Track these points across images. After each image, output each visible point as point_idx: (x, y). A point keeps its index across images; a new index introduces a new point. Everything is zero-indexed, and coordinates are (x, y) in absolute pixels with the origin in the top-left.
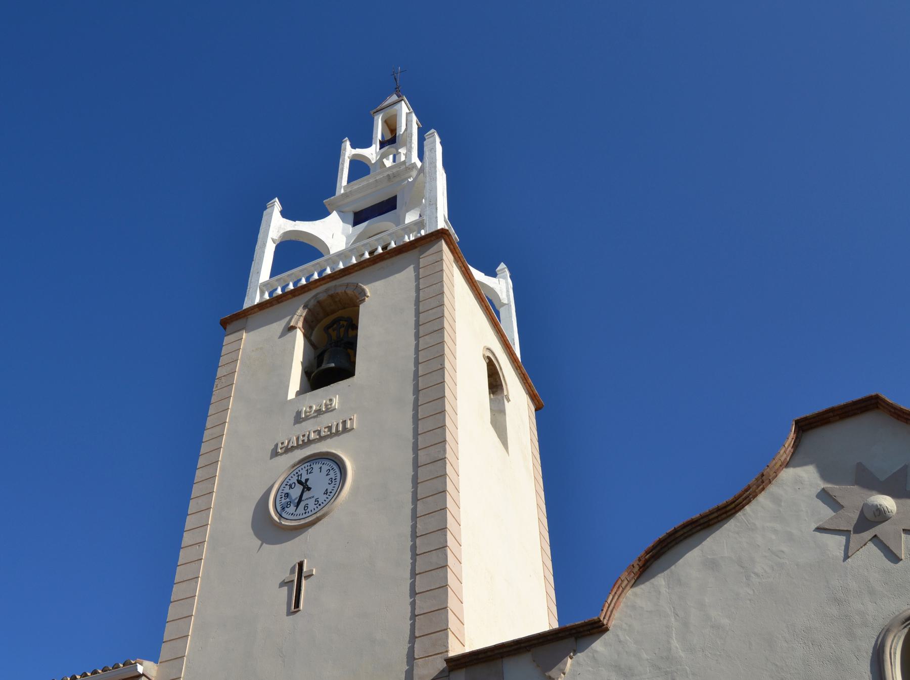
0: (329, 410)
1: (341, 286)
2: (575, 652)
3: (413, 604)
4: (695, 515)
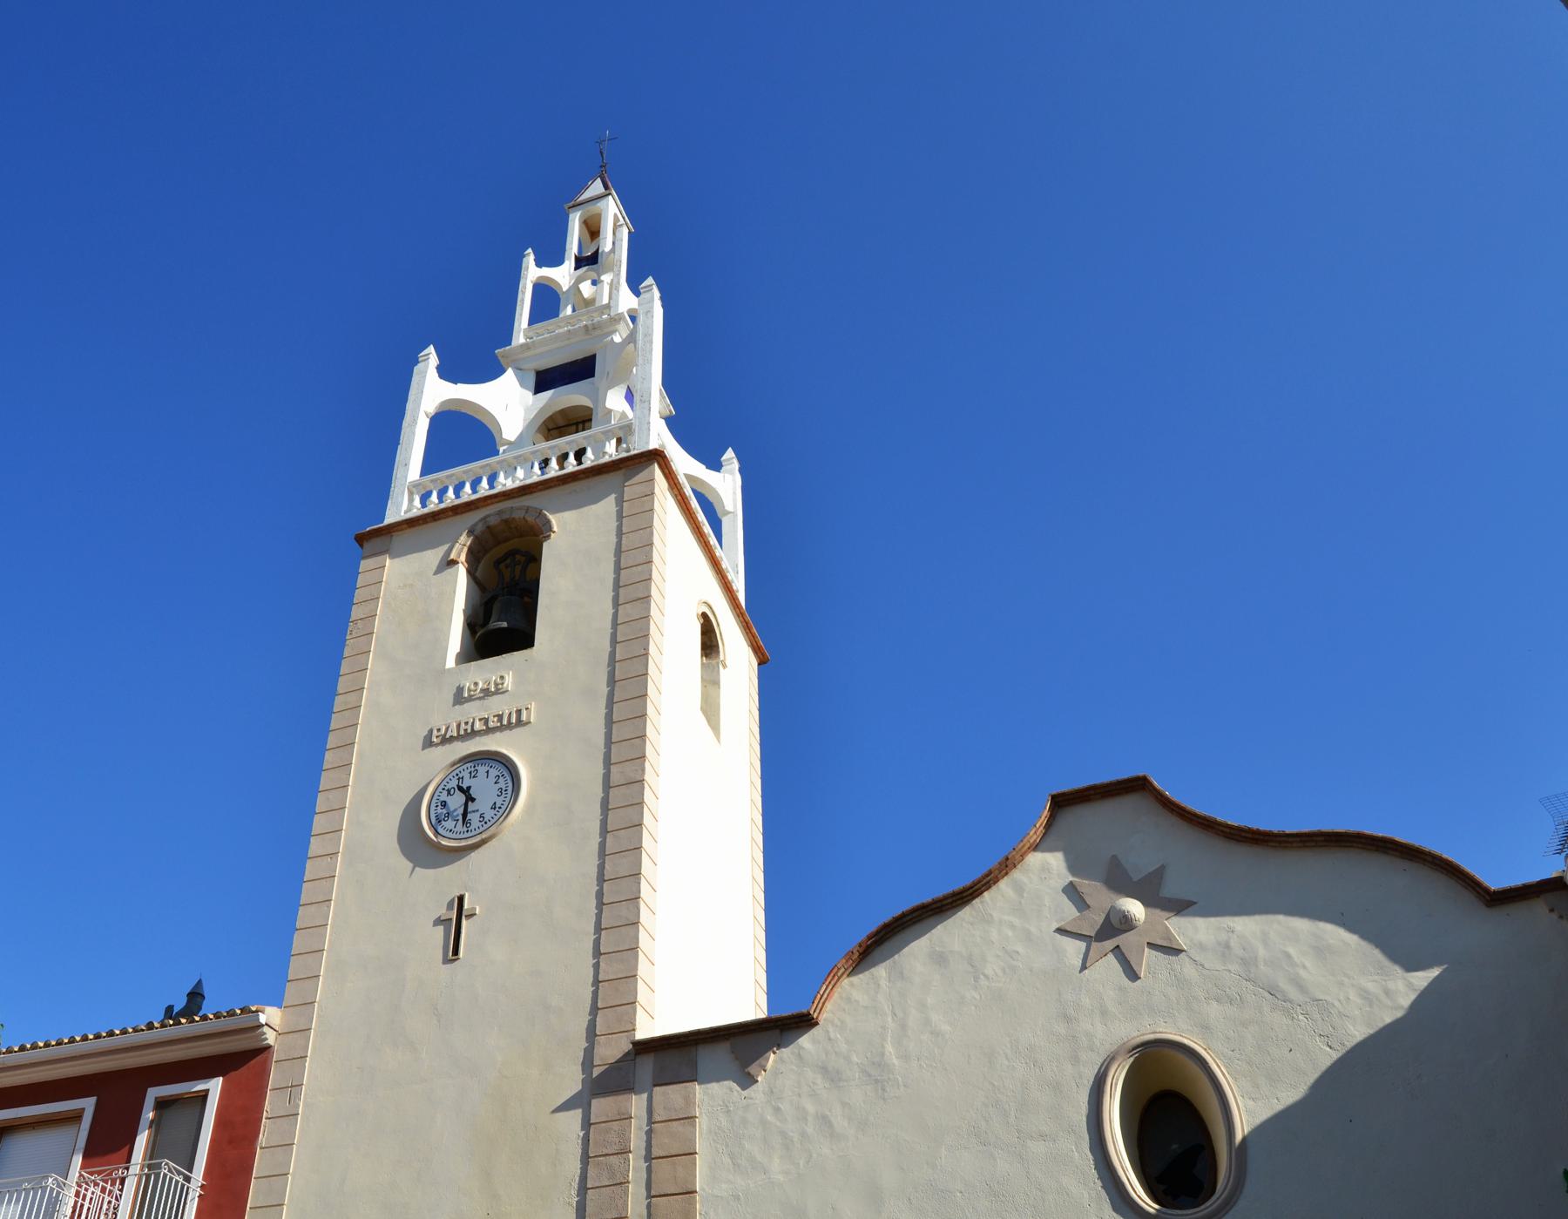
1: (520, 508)
2: (779, 1047)
3: (596, 967)
4: (927, 899)
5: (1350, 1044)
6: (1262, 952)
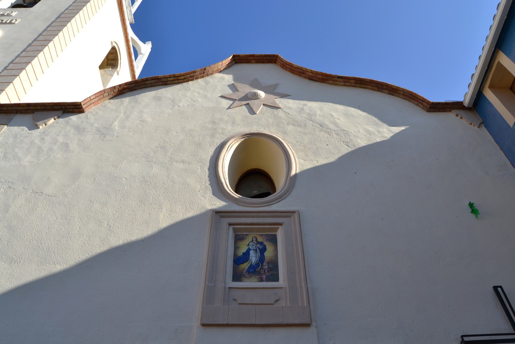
0: (8, 15)
2: (59, 117)
5: (357, 147)
6: (318, 112)
